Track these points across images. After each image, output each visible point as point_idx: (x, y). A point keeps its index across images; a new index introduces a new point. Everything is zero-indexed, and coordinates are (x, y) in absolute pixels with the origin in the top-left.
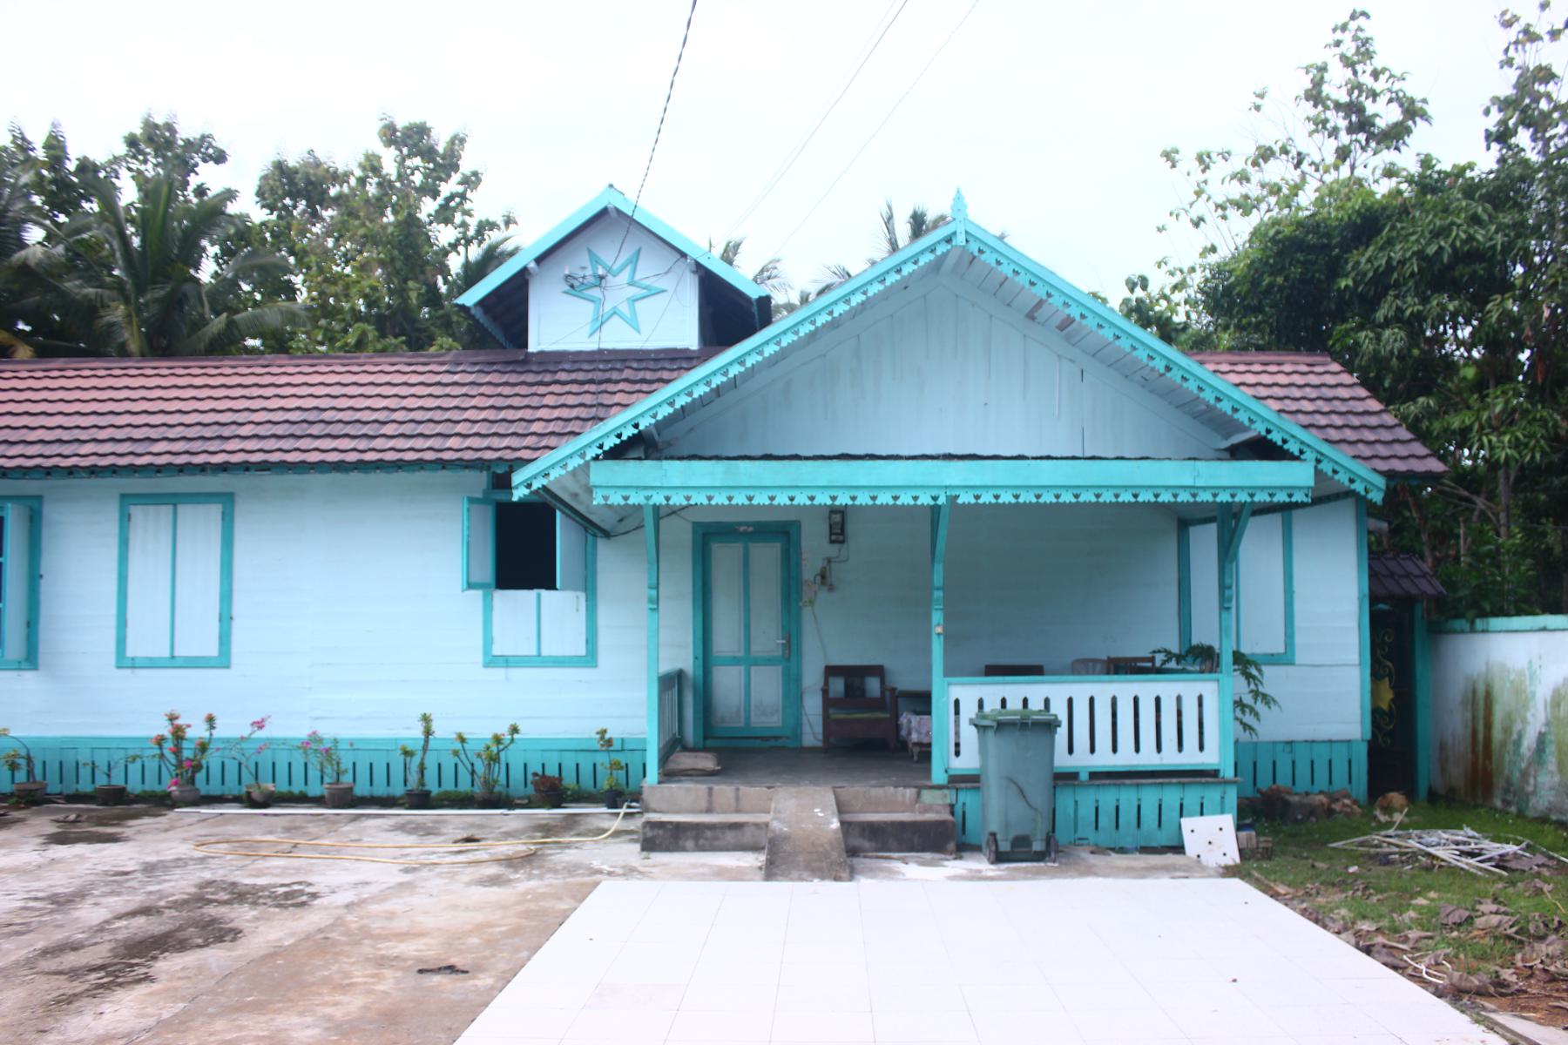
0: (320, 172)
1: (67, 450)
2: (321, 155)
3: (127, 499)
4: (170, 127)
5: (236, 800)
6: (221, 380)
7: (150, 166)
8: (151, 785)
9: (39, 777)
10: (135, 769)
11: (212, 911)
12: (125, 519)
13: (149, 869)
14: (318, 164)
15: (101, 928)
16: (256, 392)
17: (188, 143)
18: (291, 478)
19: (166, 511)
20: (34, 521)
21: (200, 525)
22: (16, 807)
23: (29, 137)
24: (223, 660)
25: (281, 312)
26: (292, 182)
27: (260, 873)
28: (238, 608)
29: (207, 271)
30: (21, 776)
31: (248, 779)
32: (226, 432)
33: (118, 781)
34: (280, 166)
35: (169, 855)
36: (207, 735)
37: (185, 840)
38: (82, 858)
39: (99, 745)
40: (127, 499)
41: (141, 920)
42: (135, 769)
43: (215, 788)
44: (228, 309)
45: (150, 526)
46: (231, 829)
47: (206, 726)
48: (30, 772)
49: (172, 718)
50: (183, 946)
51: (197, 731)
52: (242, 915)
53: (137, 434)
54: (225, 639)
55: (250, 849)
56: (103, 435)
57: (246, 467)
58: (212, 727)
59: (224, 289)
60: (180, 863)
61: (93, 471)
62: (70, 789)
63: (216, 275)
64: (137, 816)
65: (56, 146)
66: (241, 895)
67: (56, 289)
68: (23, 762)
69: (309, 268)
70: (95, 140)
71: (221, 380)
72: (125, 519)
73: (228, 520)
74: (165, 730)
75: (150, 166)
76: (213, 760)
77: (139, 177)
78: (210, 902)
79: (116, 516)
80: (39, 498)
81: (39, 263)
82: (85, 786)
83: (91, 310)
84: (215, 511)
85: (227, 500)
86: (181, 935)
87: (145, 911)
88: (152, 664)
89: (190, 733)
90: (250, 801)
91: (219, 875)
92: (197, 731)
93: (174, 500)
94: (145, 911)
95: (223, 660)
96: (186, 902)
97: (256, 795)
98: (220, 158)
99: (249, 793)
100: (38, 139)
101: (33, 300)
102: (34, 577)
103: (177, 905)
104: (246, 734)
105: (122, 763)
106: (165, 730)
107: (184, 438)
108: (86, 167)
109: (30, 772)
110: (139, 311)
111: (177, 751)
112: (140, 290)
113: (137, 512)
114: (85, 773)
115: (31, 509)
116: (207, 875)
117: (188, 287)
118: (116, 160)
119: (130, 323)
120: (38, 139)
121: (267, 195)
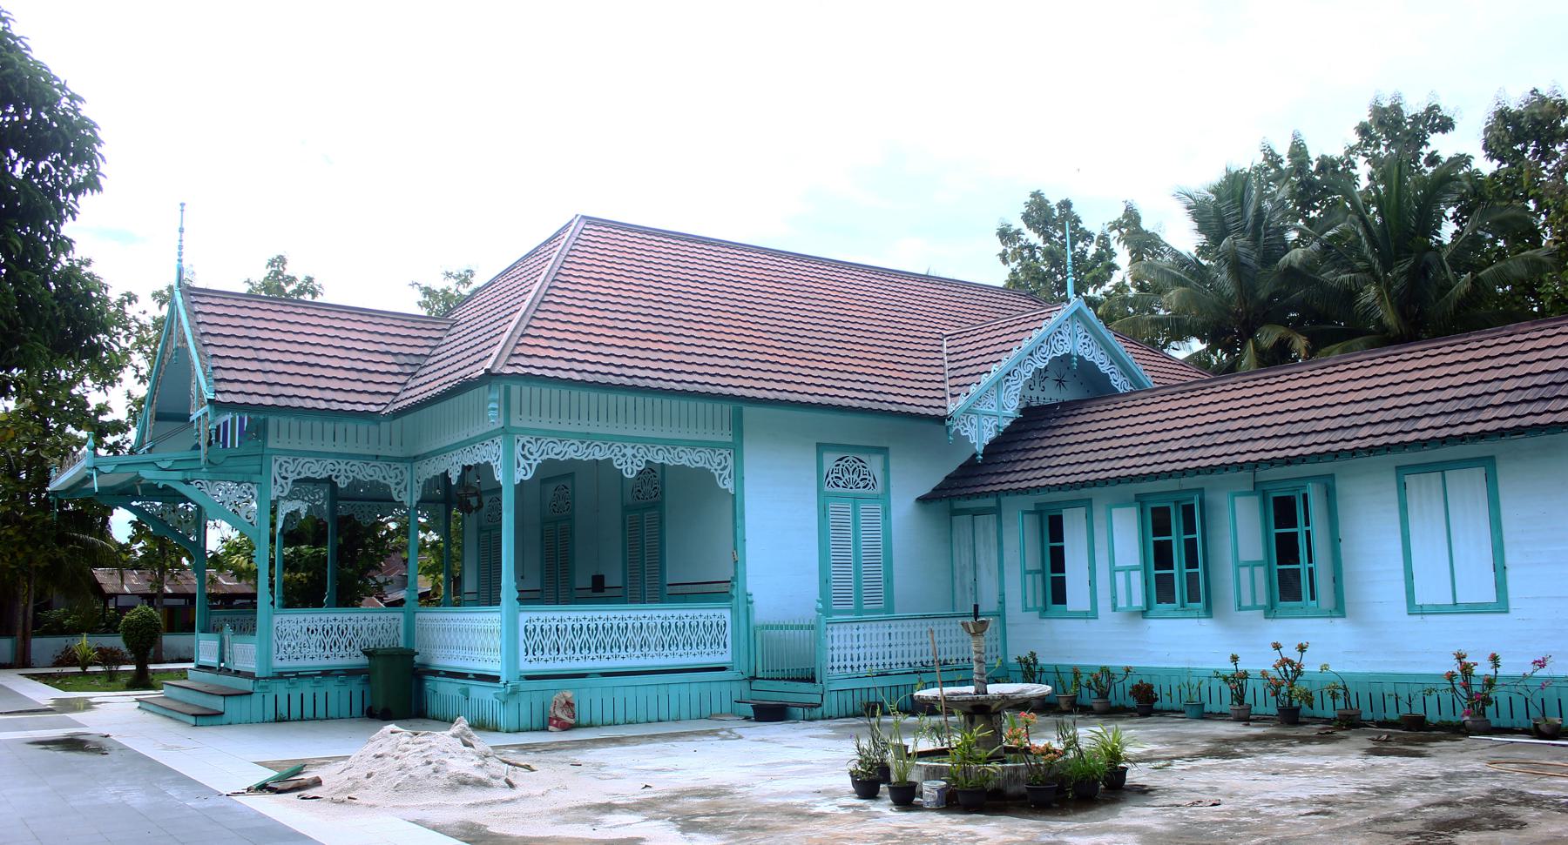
0: (1547, 108)
1: (1348, 434)
2: (1544, 91)
3: (1402, 471)
4: (1396, 108)
5: (1525, 732)
6: (1471, 355)
7: (1382, 149)
8: (1447, 716)
9: (1354, 705)
10: (1431, 700)
11: (1502, 808)
12: (1402, 487)
13: (1449, 777)
14: (1543, 100)
15: (1415, 811)
16: (1503, 361)
17: (1416, 119)
18: (1545, 439)
19: (1435, 478)
20: (1330, 495)
21: (1467, 488)
22: (1340, 728)
23: (1278, 152)
24: (1501, 605)
25: (1526, 263)
26: (1517, 126)
27: (1545, 787)
28: (1509, 559)
29: (1448, 231)
30: (1340, 704)
31: (1534, 713)
32: (1480, 403)
33: (1418, 710)
34: (1503, 116)
35: (1465, 769)
36: (1492, 672)
37: (1478, 759)
38: (1395, 765)
39: (1400, 680)
40: (1402, 471)
41: (1445, 809)
42: (1431, 700)
43: (1505, 721)
44: (1470, 267)
45: (1423, 490)
46: (1520, 754)
47: (1491, 664)
48: (1347, 700)
49: (1460, 657)
50: (1478, 828)
51: (1483, 669)
52: (1529, 814)
53: (1403, 414)
54: (1501, 586)
55: (1537, 770)
56: (1375, 418)
57: (1501, 433)
58: (1496, 665)
59: (1467, 245)
60: (1473, 774)
61: (1371, 450)
62: (1380, 717)
63: (1456, 234)
64: (1437, 740)
65: (1298, 151)
66: (1526, 800)
67: (1316, 281)
68: (1341, 692)
69: (1548, 207)
70: (1331, 138)
71: (1471, 355)
72: (1402, 487)
73: (1089, 518)
74: (1455, 668)
75: (1382, 149)
76: (1499, 694)
77: (1374, 161)
78: (1500, 803)
79: (1394, 485)
80: (1332, 476)
81: (1301, 263)
82: (1392, 715)
83: (1349, 295)
84: (1478, 474)
85: (1488, 463)
86: (1477, 821)
87: (1448, 804)
88: (1438, 610)
89: (1476, 671)
90: (1536, 732)
91: (1509, 785)
92: (1483, 669)
93: (1442, 467)
94: (1448, 804)
95: (1501, 605)
96: (1478, 801)
97: (1543, 727)
98: (1446, 125)
99: (1536, 726)
100: (1283, 150)
101: (1299, 294)
102: (1335, 541)
103: (1471, 802)
104: (1528, 672)
105: (1421, 695)
106: (1455, 668)
107: (1443, 413)
108: (1326, 165)
109: (1347, 700)
110: (1389, 286)
111: (1467, 686)
112: (1387, 267)
113: (1411, 480)
114: (1390, 703)
115: (1327, 486)
116: (1498, 785)
117: (1430, 256)
118: (1351, 150)
119: (1382, 300)
120: (1283, 150)
121: (1493, 148)
